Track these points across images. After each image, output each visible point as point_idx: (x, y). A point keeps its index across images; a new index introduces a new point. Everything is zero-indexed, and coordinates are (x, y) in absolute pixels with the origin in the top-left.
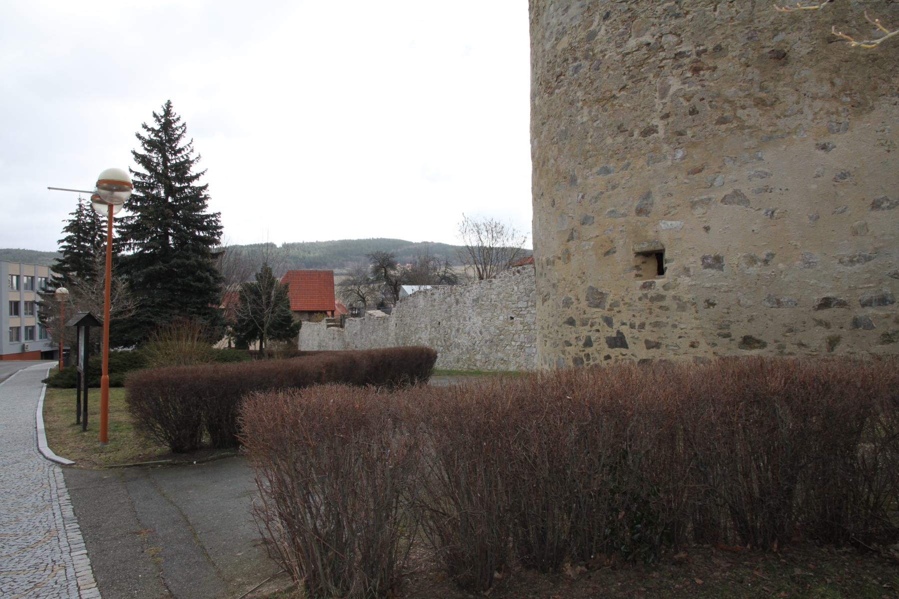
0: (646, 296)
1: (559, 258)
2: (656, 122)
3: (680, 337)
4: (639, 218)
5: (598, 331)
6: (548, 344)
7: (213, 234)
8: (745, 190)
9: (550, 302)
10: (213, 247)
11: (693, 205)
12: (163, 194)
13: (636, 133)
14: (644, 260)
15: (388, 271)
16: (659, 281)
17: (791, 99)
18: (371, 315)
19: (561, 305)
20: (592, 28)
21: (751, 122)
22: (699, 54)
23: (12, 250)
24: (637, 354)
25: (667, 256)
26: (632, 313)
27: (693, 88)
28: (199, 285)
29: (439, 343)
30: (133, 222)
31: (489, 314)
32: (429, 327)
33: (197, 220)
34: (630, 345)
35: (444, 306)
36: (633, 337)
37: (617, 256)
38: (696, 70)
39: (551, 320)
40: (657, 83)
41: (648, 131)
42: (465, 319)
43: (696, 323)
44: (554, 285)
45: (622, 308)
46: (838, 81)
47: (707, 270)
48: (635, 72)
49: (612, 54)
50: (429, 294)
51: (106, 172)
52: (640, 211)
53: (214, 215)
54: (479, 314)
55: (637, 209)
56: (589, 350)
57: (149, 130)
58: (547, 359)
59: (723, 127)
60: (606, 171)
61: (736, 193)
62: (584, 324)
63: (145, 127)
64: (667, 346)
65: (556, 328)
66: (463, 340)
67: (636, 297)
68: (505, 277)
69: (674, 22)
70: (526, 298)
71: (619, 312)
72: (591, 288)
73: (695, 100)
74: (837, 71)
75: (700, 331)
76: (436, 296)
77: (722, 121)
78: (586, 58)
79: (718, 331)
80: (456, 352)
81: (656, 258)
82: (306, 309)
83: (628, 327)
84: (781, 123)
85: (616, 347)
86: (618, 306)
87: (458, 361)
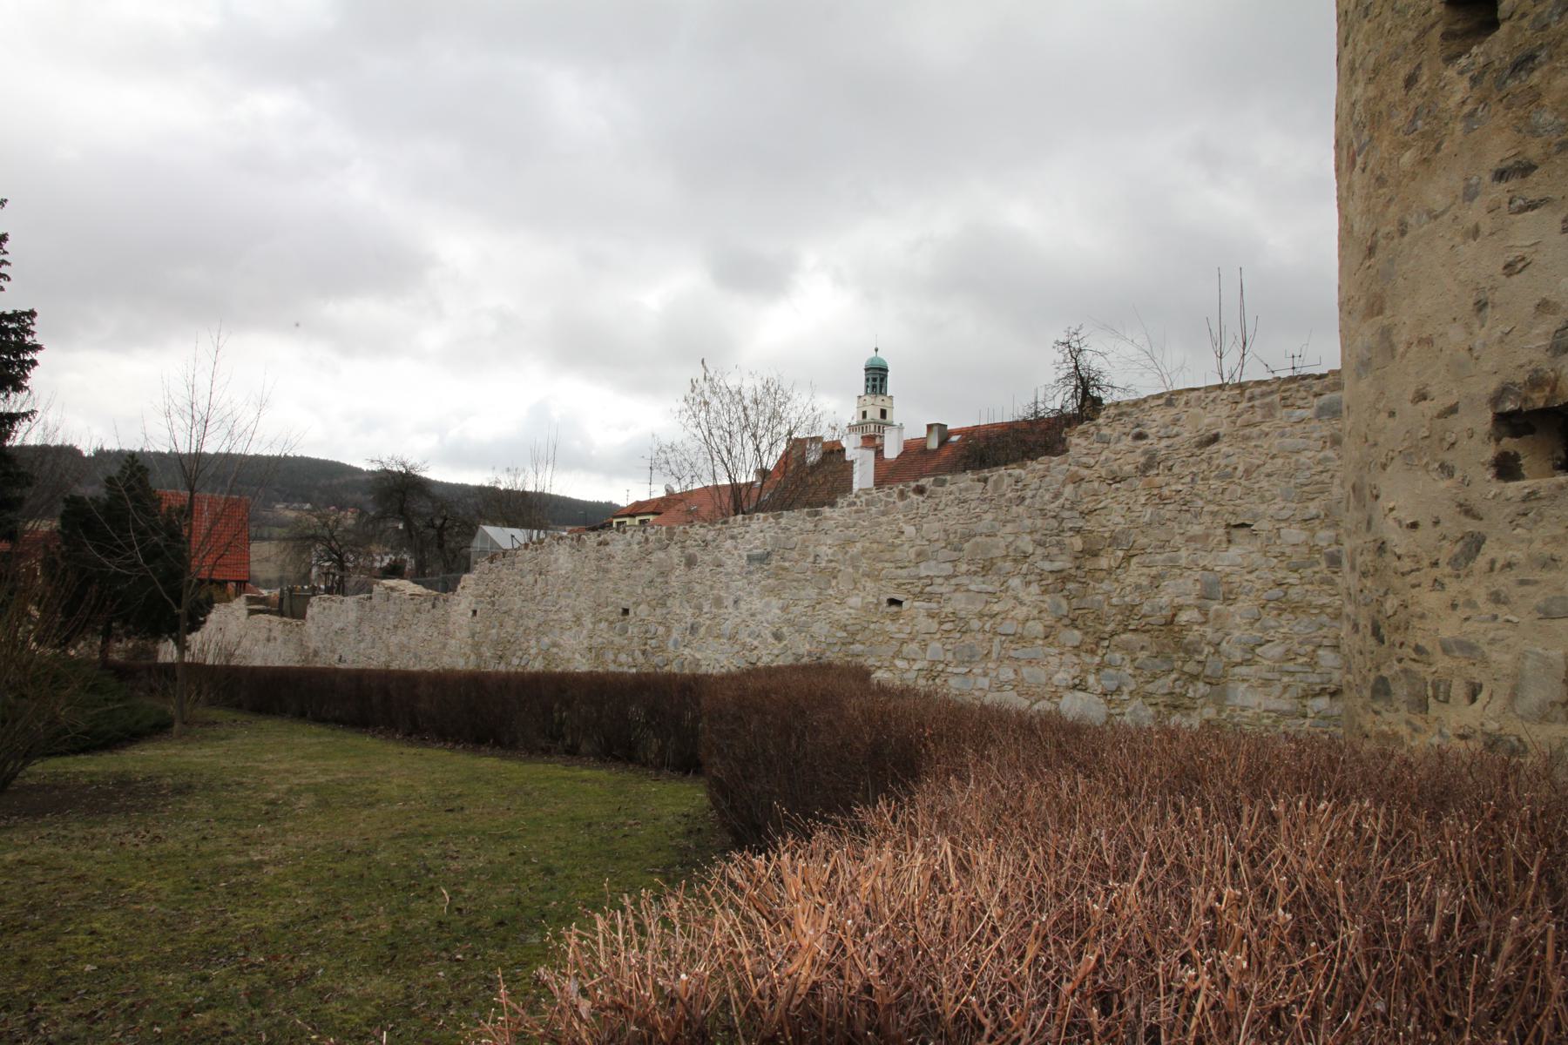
23: (409, 680)
32: (587, 621)
53: (15, 317)
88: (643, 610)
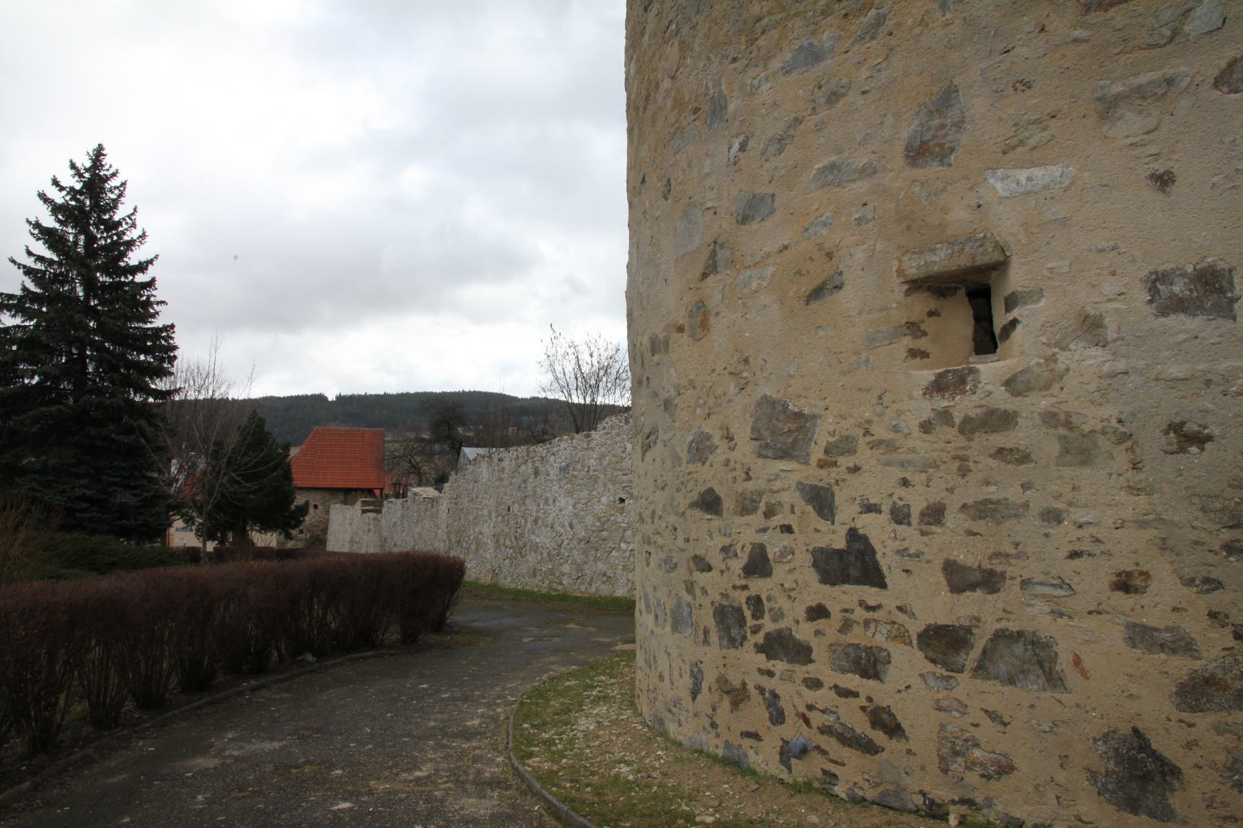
0: (945, 416)
1: (681, 329)
3: (1074, 555)
4: (917, 173)
5: (787, 529)
6: (654, 562)
7: (162, 360)
9: (658, 450)
10: (161, 385)
11: (1108, 107)
12: (80, 292)
14: (933, 304)
15: (447, 429)
16: (990, 370)
18: (415, 494)
19: (684, 455)
25: (1016, 279)
26: (898, 473)
28: (123, 438)
29: (508, 542)
31: (585, 493)
32: (494, 515)
33: (133, 337)
34: (893, 577)
35: (517, 480)
36: (902, 552)
37: (847, 299)
39: (660, 497)
42: (546, 503)
43: (1132, 506)
44: (667, 404)
45: (865, 456)
47: (1175, 321)
52: (918, 153)
54: (569, 493)
55: (908, 148)
56: (759, 586)
57: (62, 189)
58: (652, 600)
62: (747, 507)
63: (56, 183)
64: (1025, 583)
65: (672, 519)
66: (543, 538)
67: (912, 423)
68: (612, 428)
71: (855, 469)
72: (767, 402)
75: (1150, 533)
76: (506, 463)
79: (1226, 535)
80: (532, 558)
81: (973, 295)
82: (341, 485)
83: (884, 517)
85: (846, 579)
86: (852, 451)
87: (534, 575)
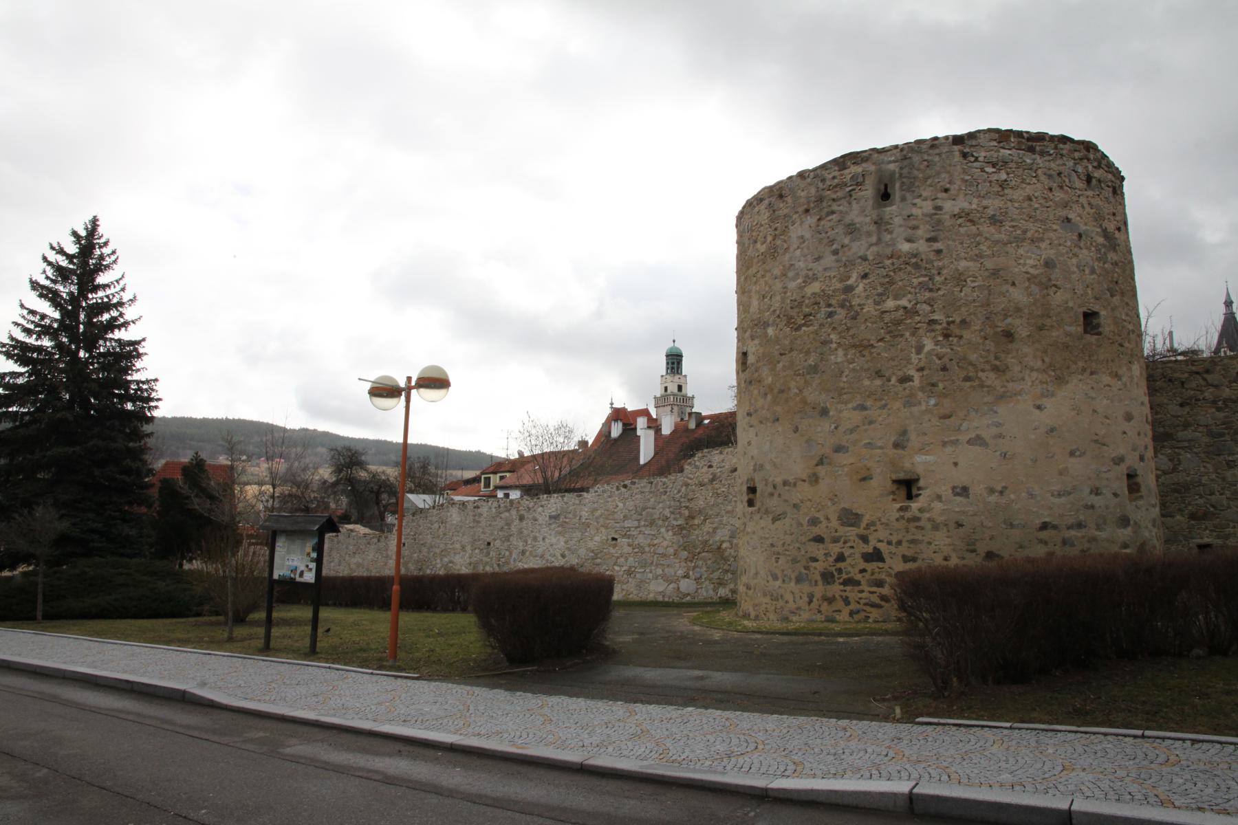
0: (902, 517)
2: (912, 372)
8: (986, 435)
11: (944, 444)
13: (894, 379)
17: (1017, 368)
20: (849, 282)
21: (989, 383)
22: (949, 323)
24: (893, 566)
27: (944, 350)
30: (20, 381)
32: (469, 548)
35: (499, 523)
38: (946, 336)
40: (913, 340)
41: (905, 379)
43: (948, 541)
45: (879, 527)
46: (1047, 359)
48: (893, 328)
49: (869, 309)
50: (470, 506)
51: (424, 370)
52: (896, 445)
53: (148, 382)
59: (968, 384)
60: (863, 408)
61: (978, 437)
67: (893, 519)
69: (927, 295)
70: (635, 517)
72: (844, 509)
73: (946, 359)
74: (1045, 352)
77: (967, 379)
78: (842, 306)
84: (1010, 385)
88: (498, 543)
